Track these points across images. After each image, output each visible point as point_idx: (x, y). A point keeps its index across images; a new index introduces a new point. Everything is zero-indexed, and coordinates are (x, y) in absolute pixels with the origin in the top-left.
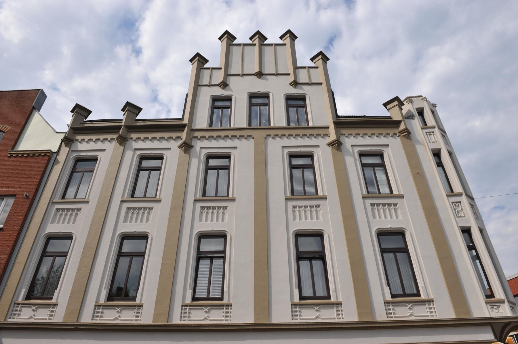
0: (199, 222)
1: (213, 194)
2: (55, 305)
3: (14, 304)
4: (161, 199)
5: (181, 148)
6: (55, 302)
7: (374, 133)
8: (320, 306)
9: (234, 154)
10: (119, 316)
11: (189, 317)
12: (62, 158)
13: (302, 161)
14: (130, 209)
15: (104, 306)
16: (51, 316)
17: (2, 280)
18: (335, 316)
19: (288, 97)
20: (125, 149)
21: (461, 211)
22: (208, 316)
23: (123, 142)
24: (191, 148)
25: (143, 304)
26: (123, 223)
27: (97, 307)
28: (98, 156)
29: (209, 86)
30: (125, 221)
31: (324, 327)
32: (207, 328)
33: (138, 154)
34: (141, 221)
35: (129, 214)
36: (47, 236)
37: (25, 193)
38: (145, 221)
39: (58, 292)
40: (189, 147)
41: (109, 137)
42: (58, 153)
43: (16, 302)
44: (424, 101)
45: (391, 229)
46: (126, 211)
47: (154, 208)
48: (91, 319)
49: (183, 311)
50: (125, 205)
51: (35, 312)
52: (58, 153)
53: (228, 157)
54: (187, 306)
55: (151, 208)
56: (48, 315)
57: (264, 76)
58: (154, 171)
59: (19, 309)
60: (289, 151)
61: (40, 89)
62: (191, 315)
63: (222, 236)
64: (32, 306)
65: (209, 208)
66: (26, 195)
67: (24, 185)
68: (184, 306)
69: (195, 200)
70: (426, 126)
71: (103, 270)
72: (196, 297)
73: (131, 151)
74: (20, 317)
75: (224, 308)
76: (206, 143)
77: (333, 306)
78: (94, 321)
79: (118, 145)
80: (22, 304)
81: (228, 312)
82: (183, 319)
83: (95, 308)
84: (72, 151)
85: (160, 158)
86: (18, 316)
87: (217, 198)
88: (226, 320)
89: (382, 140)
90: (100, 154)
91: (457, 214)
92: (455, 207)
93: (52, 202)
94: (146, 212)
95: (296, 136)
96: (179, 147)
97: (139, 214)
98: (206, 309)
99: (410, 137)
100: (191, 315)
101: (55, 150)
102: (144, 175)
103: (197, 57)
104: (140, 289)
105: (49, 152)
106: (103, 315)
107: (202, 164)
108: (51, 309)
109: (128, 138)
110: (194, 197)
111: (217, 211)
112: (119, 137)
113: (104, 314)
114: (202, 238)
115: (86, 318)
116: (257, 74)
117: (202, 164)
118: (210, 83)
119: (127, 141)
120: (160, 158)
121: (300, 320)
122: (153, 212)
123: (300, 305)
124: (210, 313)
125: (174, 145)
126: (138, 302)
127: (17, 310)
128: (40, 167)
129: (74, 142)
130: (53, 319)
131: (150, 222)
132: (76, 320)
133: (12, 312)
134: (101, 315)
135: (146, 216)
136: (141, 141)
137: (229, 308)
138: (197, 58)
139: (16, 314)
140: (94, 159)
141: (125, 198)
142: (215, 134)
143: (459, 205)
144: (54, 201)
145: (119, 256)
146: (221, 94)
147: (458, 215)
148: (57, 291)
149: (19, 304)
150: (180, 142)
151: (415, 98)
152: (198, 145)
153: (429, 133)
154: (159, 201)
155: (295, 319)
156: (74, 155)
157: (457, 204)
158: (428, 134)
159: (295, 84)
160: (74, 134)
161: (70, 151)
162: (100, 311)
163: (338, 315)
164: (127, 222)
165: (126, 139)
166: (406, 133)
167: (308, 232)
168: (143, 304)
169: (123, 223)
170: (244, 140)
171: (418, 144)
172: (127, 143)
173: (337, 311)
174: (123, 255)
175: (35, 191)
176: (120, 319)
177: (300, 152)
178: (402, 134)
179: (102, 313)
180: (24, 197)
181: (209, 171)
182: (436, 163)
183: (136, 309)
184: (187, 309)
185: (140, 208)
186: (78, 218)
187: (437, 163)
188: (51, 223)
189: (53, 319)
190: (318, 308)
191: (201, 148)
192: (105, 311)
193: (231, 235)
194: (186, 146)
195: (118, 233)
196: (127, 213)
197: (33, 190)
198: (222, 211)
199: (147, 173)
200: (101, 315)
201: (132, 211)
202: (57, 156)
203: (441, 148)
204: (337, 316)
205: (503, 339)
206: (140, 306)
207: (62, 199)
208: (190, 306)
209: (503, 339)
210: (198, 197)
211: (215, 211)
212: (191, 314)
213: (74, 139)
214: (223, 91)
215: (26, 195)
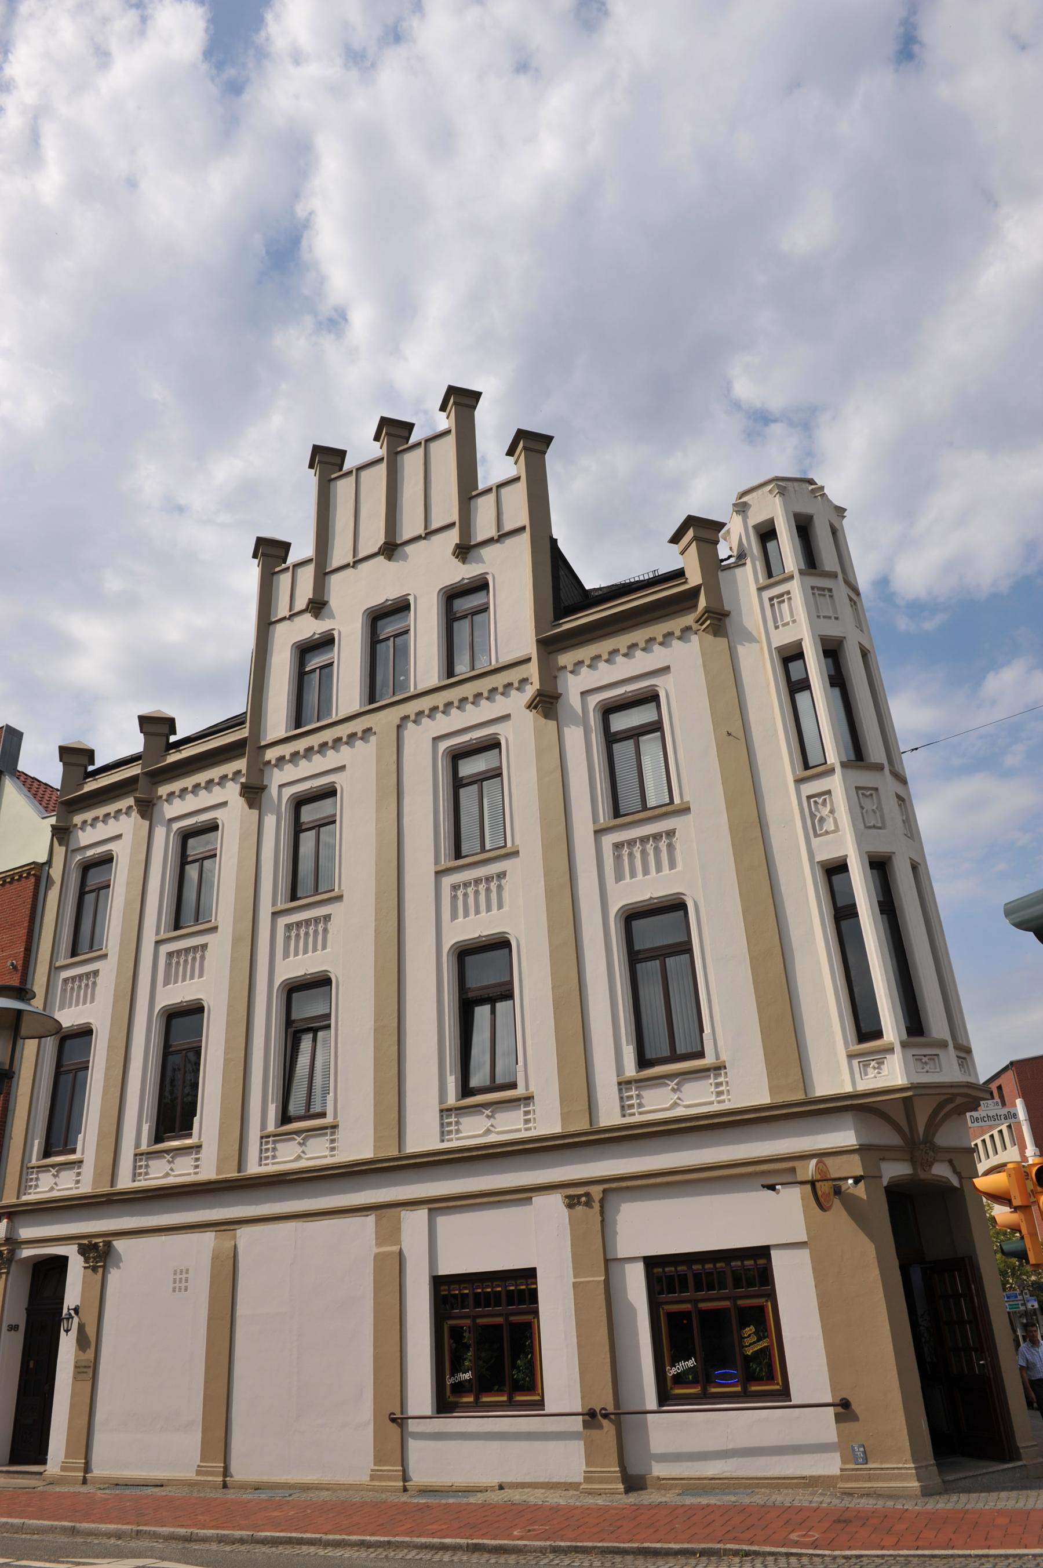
0: (284, 960)
1: (635, 803)
2: (198, 1147)
3: (25, 1169)
4: (687, 806)
5: (535, 708)
6: (634, 1076)
7: (634, 642)
8: (494, 1107)
9: (664, 685)
10: (172, 1170)
11: (640, 1105)
12: (56, 872)
13: (484, 761)
14: (658, 838)
15: (148, 1153)
16: (333, 1149)
17: (4, 1130)
18: (521, 1126)
19: (449, 595)
20: (153, 826)
21: (829, 817)
22: (679, 1099)
23: (146, 811)
24: (262, 792)
25: (533, 1092)
26: (616, 883)
27: (138, 1157)
28: (498, 736)
29: (497, 541)
30: (619, 877)
31: (491, 1151)
32: (295, 1177)
33: (175, 830)
34: (659, 869)
35: (624, 860)
36: (285, 986)
37: (9, 963)
38: (668, 868)
39: (333, 1099)
40: (258, 792)
41: (676, 624)
42: (49, 862)
43: (30, 1165)
44: (775, 496)
45: (480, 939)
46: (614, 854)
47: (507, 873)
48: (439, 1141)
49: (264, 1147)
50: (609, 840)
51: (57, 1178)
52: (49, 862)
53: (651, 698)
54: (268, 1137)
55: (502, 875)
56: (327, 1148)
57: (400, 549)
58: (324, 828)
59: (34, 1176)
60: (600, 701)
61: (3, 727)
62: (461, 1127)
63: (676, 906)
64: (51, 1169)
65: (645, 840)
66: (12, 964)
67: (8, 945)
68: (624, 1084)
69: (596, 832)
70: (812, 568)
71: (139, 1087)
72: (669, 1054)
73: (162, 826)
74: (38, 1190)
75: (327, 1133)
76: (289, 773)
77: (73, 1165)
78: (137, 1184)
79: (709, 638)
80: (38, 1167)
81: (721, 1084)
82: (264, 1162)
83: (135, 1161)
84: (73, 851)
85: (493, 745)
86: (35, 1189)
87: (645, 812)
88: (719, 1102)
89: (642, 662)
90: (503, 731)
91: (815, 826)
92: (813, 809)
93: (54, 969)
94: (493, 886)
95: (577, 667)
96: (528, 707)
97: (492, 891)
98: (672, 1082)
99: (726, 628)
100: (461, 1127)
101: (43, 858)
102: (467, 795)
103: (522, 442)
104: (707, 1029)
105: (33, 866)
106: (277, 1153)
107: (593, 736)
108: (194, 1156)
109: (153, 798)
110: (594, 822)
111: (641, 848)
112: (706, 615)
113: (461, 1124)
114: (634, 920)
115: (125, 1182)
116: (384, 551)
117: (593, 736)
118: (498, 531)
119: (154, 805)
120: (493, 745)
121: (641, 1116)
122: (678, 841)
123: (637, 1081)
124: (681, 1092)
125: (232, 792)
126: (709, 1060)
127: (32, 1179)
128: (24, 903)
129: (71, 832)
130: (729, 1100)
131: (506, 908)
132: (236, 1168)
133: (26, 1182)
134: (638, 1101)
135: (495, 895)
136: (218, 787)
137: (710, 1076)
138: (521, 445)
139: (31, 1186)
140: (329, 792)
141: (445, 864)
142: (468, 690)
143: (825, 800)
144: (58, 964)
145: (634, 962)
146: (461, 578)
147: (821, 828)
148: (196, 1120)
149: (33, 1168)
150: (530, 691)
151: (754, 494)
152: (277, 777)
153: (819, 588)
154: (515, 854)
155: (448, 1140)
156: (77, 859)
157: (820, 800)
158: (816, 591)
159: (464, 551)
160: (549, 653)
161: (69, 853)
162: (633, 1093)
163: (527, 1121)
164: (624, 879)
165: (150, 802)
166: (708, 622)
167: (306, 979)
168: (533, 1092)
169: (616, 883)
170: (359, 743)
171: (744, 643)
172: (156, 809)
173: (527, 1113)
174: (640, 957)
175: (25, 954)
176: (173, 1173)
177: (471, 742)
178: (702, 624)
179: (639, 1096)
180: (10, 969)
181: (616, 747)
182: (829, 675)
183: (522, 1106)
184: (269, 1142)
185: (187, 950)
186: (506, 895)
187: (830, 677)
188: (59, 1010)
189: (535, 1128)
190: (490, 1112)
191: (582, 693)
192: (151, 1163)
193: (694, 899)
194: (545, 702)
195: (613, 910)
196: (618, 858)
197: (21, 952)
198: (652, 845)
199: (475, 788)
200: (638, 1101)
201: (625, 851)
202: (50, 870)
203: (802, 639)
204: (717, 1097)
205: (939, 1118)
206: (528, 1099)
207: (174, 930)
208: (275, 1136)
209: (939, 1118)
210: (602, 821)
211: (650, 847)
212: (643, 1098)
213: (70, 826)
214: (466, 566)
215: (12, 964)
